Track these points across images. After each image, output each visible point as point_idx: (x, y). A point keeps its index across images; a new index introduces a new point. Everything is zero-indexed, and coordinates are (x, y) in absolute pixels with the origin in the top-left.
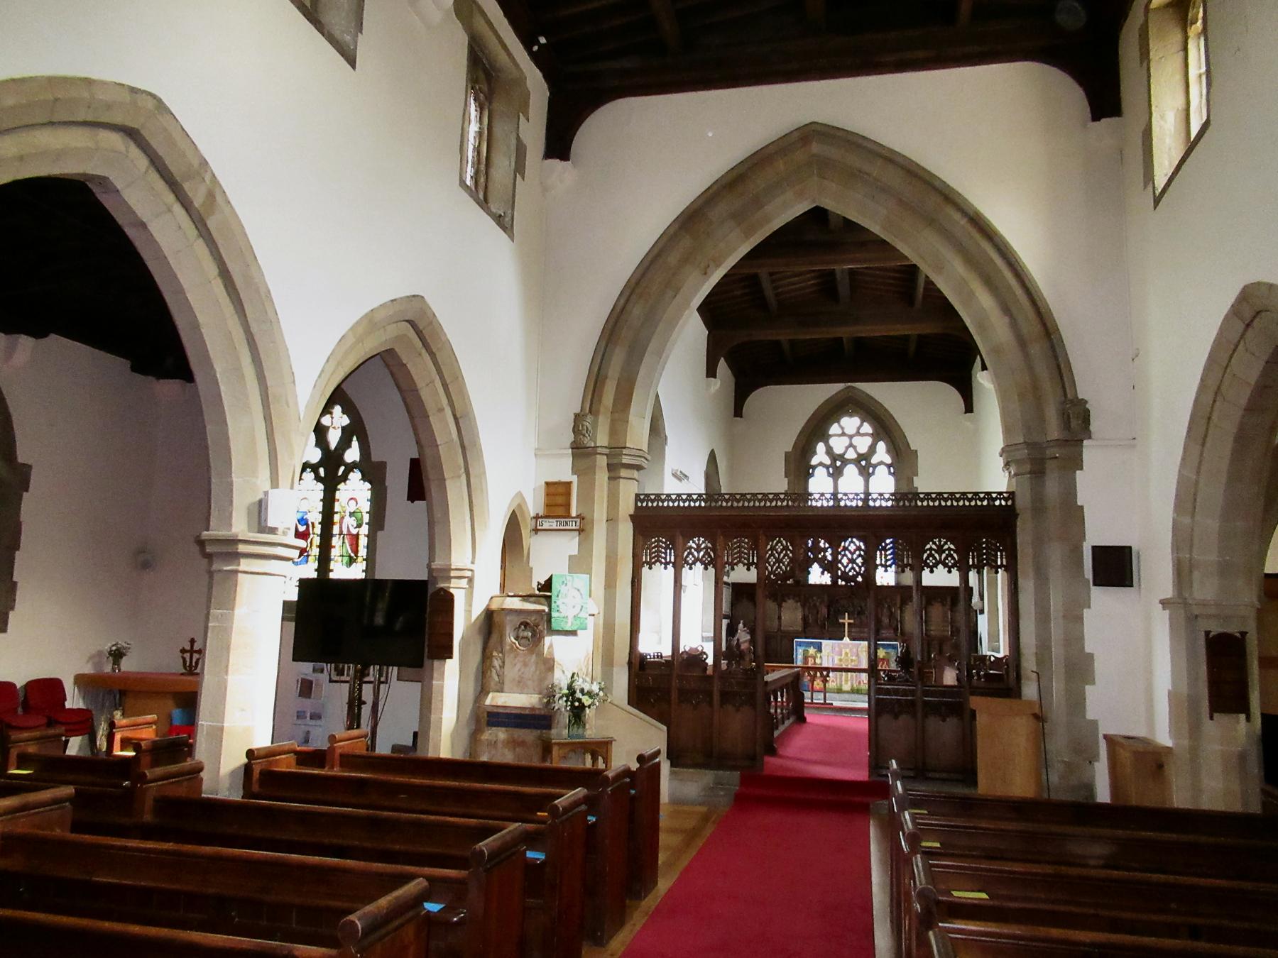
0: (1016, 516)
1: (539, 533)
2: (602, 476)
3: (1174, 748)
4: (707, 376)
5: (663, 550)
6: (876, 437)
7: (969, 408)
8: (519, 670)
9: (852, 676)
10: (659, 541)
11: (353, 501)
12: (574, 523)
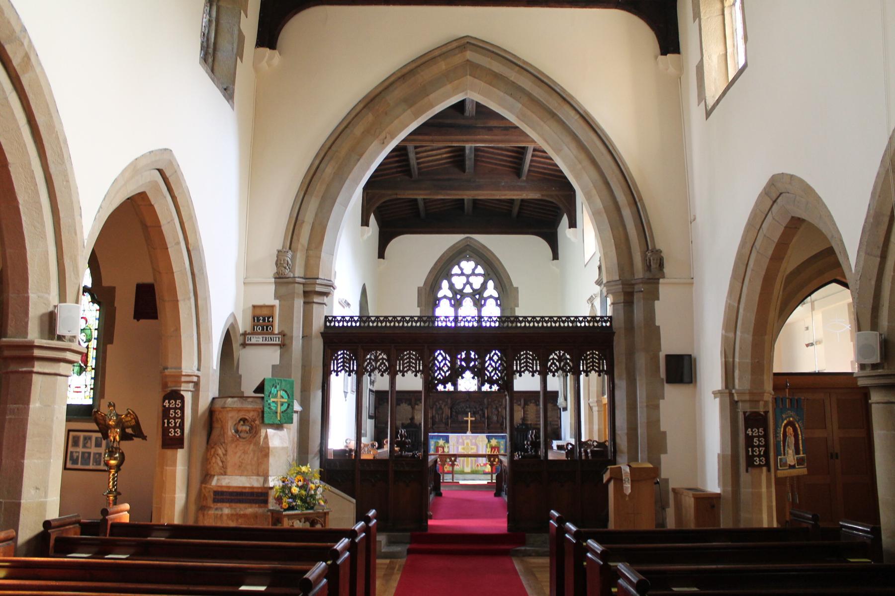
0: (613, 333)
1: (247, 347)
2: (299, 303)
3: (722, 493)
4: (362, 225)
6: (487, 277)
7: (555, 256)
8: (240, 457)
9: (472, 461)
11: (83, 320)
12: (277, 339)
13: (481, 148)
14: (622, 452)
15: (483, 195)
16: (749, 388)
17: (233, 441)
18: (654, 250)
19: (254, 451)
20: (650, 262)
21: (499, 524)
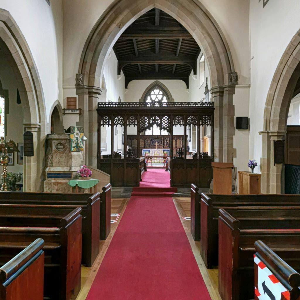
0: (214, 109)
1: (66, 115)
2: (86, 97)
4: (118, 74)
5: (107, 121)
6: (163, 95)
7: (188, 87)
8: (58, 159)
10: (132, 118)
13: (162, 40)
14: (217, 157)
15: (162, 63)
16: (277, 130)
17: (55, 152)
18: (234, 73)
19: (65, 157)
20: (232, 78)
21: (168, 186)
